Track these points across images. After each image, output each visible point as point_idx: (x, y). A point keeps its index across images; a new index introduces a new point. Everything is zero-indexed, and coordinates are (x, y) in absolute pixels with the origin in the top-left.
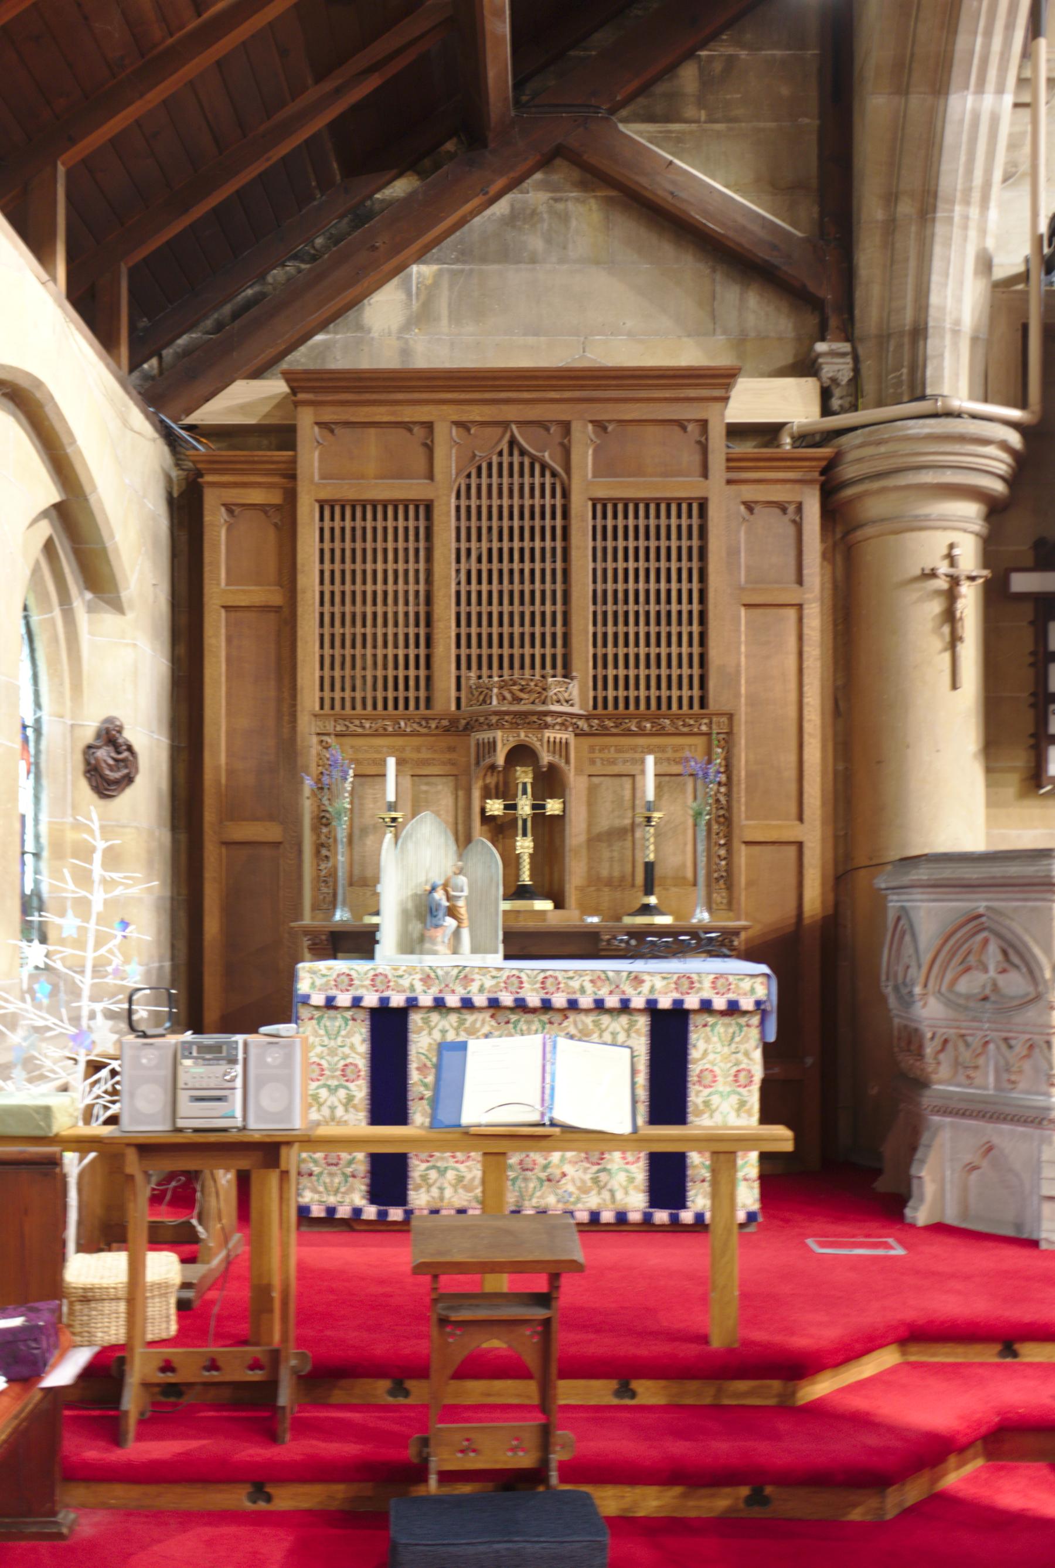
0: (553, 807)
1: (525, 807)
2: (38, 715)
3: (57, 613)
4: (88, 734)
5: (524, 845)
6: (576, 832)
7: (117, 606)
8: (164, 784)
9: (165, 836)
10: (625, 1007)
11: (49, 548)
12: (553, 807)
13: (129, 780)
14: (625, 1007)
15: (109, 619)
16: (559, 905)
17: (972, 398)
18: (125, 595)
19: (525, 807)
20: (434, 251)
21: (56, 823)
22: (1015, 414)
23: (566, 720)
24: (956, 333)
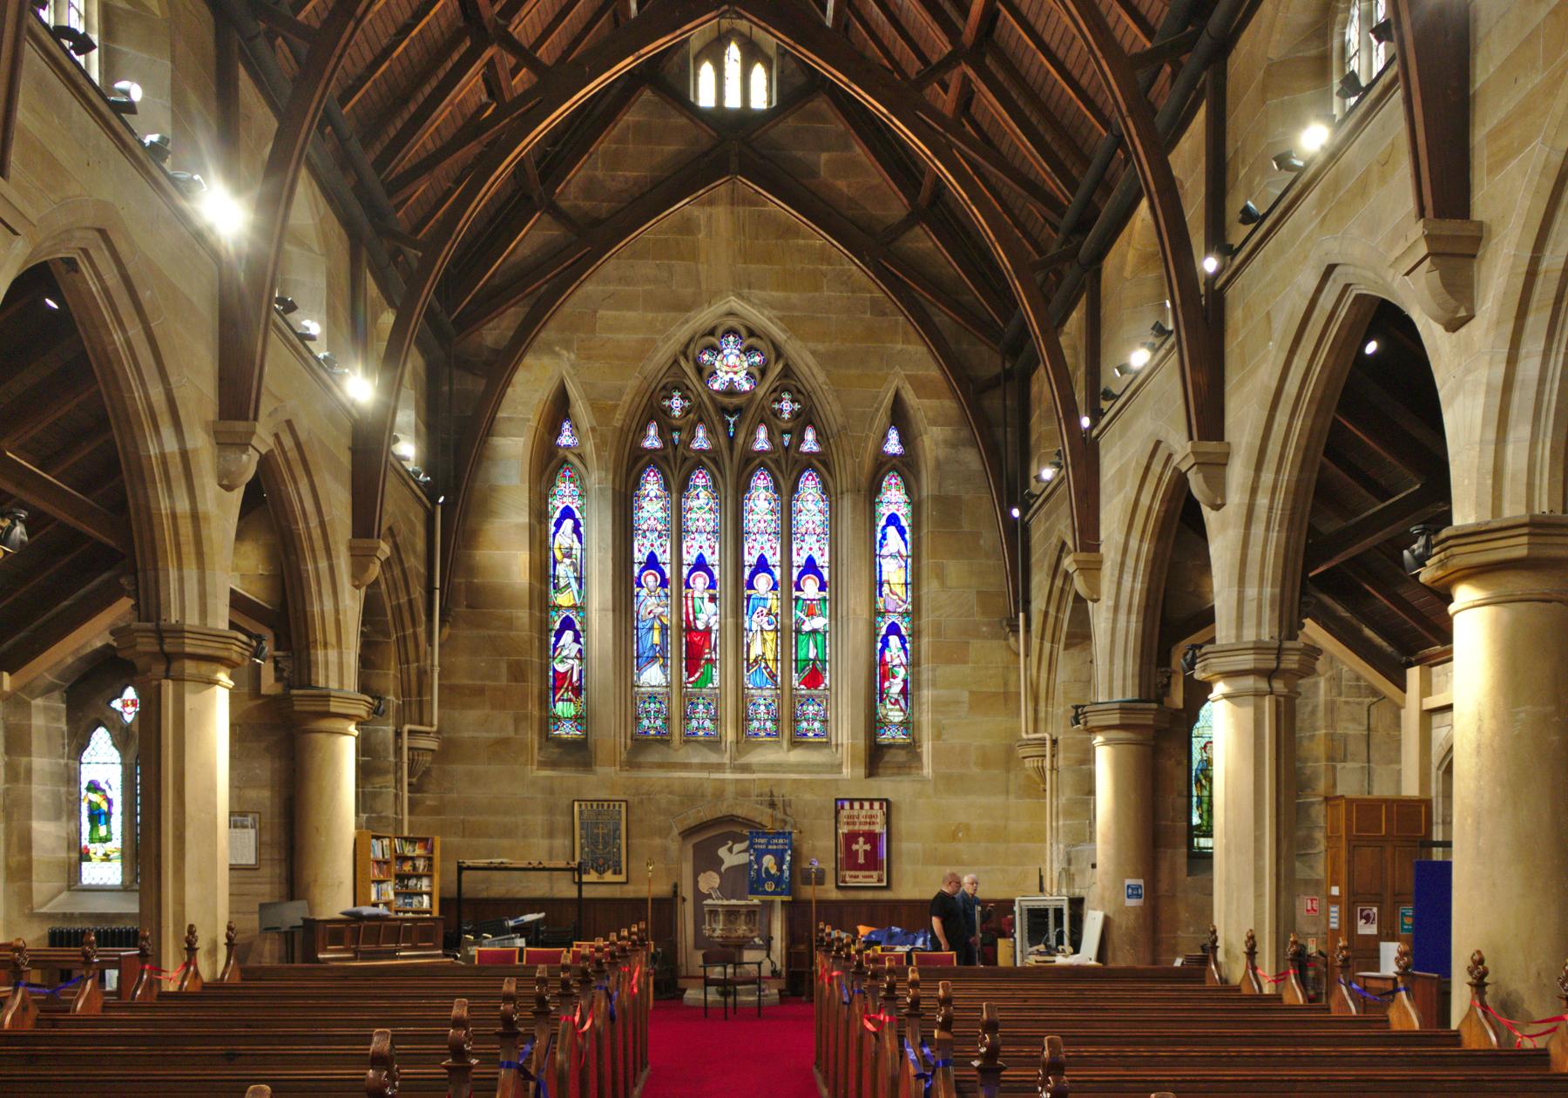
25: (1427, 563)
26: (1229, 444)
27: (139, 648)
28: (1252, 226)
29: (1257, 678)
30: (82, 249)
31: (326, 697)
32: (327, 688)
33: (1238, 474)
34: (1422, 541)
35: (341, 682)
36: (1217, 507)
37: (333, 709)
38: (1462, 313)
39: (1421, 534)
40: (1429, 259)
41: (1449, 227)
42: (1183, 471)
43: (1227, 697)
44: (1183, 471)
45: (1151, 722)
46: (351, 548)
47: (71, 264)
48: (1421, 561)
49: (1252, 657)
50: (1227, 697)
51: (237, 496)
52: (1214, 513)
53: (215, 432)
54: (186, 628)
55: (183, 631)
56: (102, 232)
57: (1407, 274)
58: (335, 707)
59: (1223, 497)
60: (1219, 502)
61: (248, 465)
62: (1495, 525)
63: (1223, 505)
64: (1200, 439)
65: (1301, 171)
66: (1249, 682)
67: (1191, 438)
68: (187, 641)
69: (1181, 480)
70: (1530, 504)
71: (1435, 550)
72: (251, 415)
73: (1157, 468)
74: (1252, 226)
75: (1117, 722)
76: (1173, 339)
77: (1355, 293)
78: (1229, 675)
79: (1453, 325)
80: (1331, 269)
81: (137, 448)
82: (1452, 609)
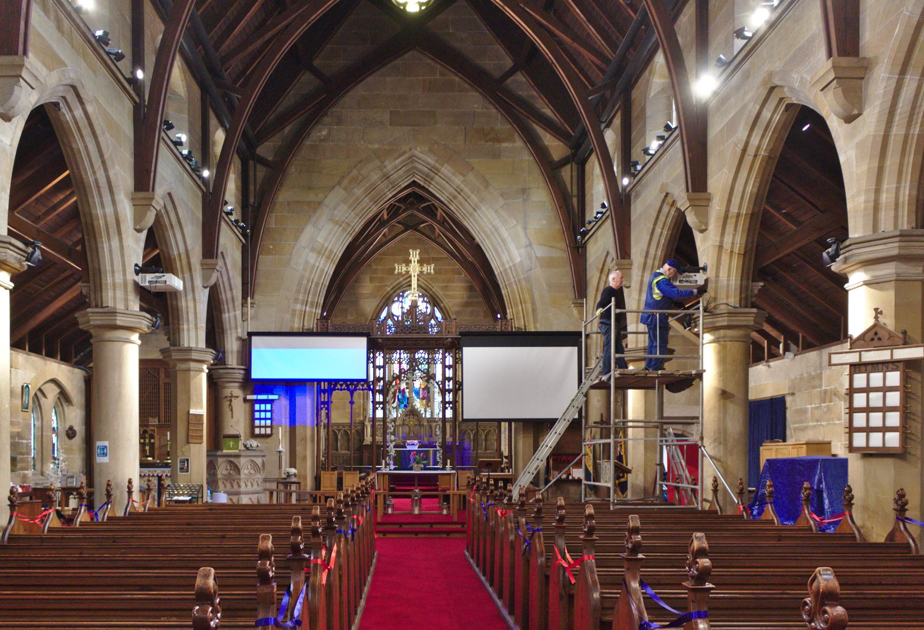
0: (152, 441)
1: (147, 441)
2: (213, 281)
3: (61, 408)
4: (67, 427)
5: (147, 448)
6: (157, 445)
7: (72, 405)
8: (84, 435)
9: (84, 446)
10: (153, 476)
11: (59, 398)
12: (152, 441)
13: (75, 436)
14: (153, 476)
15: (71, 408)
16: (154, 458)
17: (237, 365)
18: (74, 403)
19: (147, 441)
20: (406, 56)
21: (507, 274)
22: (243, 367)
23: (153, 426)
24: (232, 352)
25: (837, 260)
26: (710, 194)
27: (92, 323)
28: (670, 132)
29: (899, 264)
30: (63, 97)
31: (114, 313)
32: (115, 308)
33: (716, 208)
34: (834, 247)
35: (197, 342)
36: (702, 231)
37: (119, 323)
38: (856, 112)
39: (834, 243)
40: (835, 81)
41: (845, 61)
42: (683, 210)
43: (867, 283)
44: (683, 210)
45: (752, 323)
46: (202, 264)
47: (56, 105)
48: (833, 258)
49: (897, 244)
50: (867, 283)
51: (144, 235)
52: (701, 235)
53: (132, 199)
54: (118, 311)
55: (116, 313)
56: (74, 88)
57: (822, 90)
58: (194, 356)
59: (707, 224)
60: (703, 227)
61: (150, 219)
62: (875, 237)
63: (706, 230)
64: (693, 191)
65: (750, 39)
66: (889, 270)
67: (688, 191)
68: (118, 318)
69: (681, 216)
70: (896, 226)
71: (842, 252)
72: (151, 190)
73: (666, 209)
74: (670, 132)
75: (895, 252)
76: (677, 132)
77: (786, 102)
78: (868, 263)
79: (849, 119)
80: (772, 89)
81: (90, 209)
82: (846, 286)
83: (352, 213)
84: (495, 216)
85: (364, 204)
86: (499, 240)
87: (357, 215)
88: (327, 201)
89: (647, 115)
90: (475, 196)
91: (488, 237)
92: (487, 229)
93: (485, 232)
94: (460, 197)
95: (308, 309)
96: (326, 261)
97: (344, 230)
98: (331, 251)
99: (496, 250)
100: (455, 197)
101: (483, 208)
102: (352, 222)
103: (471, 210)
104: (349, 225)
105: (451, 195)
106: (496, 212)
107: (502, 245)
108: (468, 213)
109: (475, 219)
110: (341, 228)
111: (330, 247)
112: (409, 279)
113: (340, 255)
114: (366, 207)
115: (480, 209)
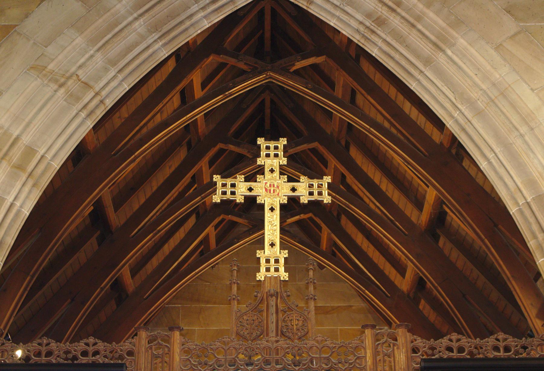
83: (99, 56)
84: (497, 58)
85: (132, 38)
86: (515, 119)
87: (113, 63)
88: (30, 25)
89: (350, 234)
90: (437, 13)
91: (479, 113)
92: (474, 95)
93: (471, 103)
94: (395, 21)
95: (140, 26)
96: (12, 177)
97: (72, 98)
98: (30, 151)
99: (508, 148)
100: (380, 22)
101: (462, 42)
102: (98, 78)
103: (426, 49)
104: (87, 86)
105: (369, 16)
106: (498, 48)
107: (523, 129)
108: (418, 56)
109: (440, 73)
110: (62, 91)
111: (26, 139)
112: (263, 236)
113: (26, 212)
114: (137, 44)
115: (452, 45)
